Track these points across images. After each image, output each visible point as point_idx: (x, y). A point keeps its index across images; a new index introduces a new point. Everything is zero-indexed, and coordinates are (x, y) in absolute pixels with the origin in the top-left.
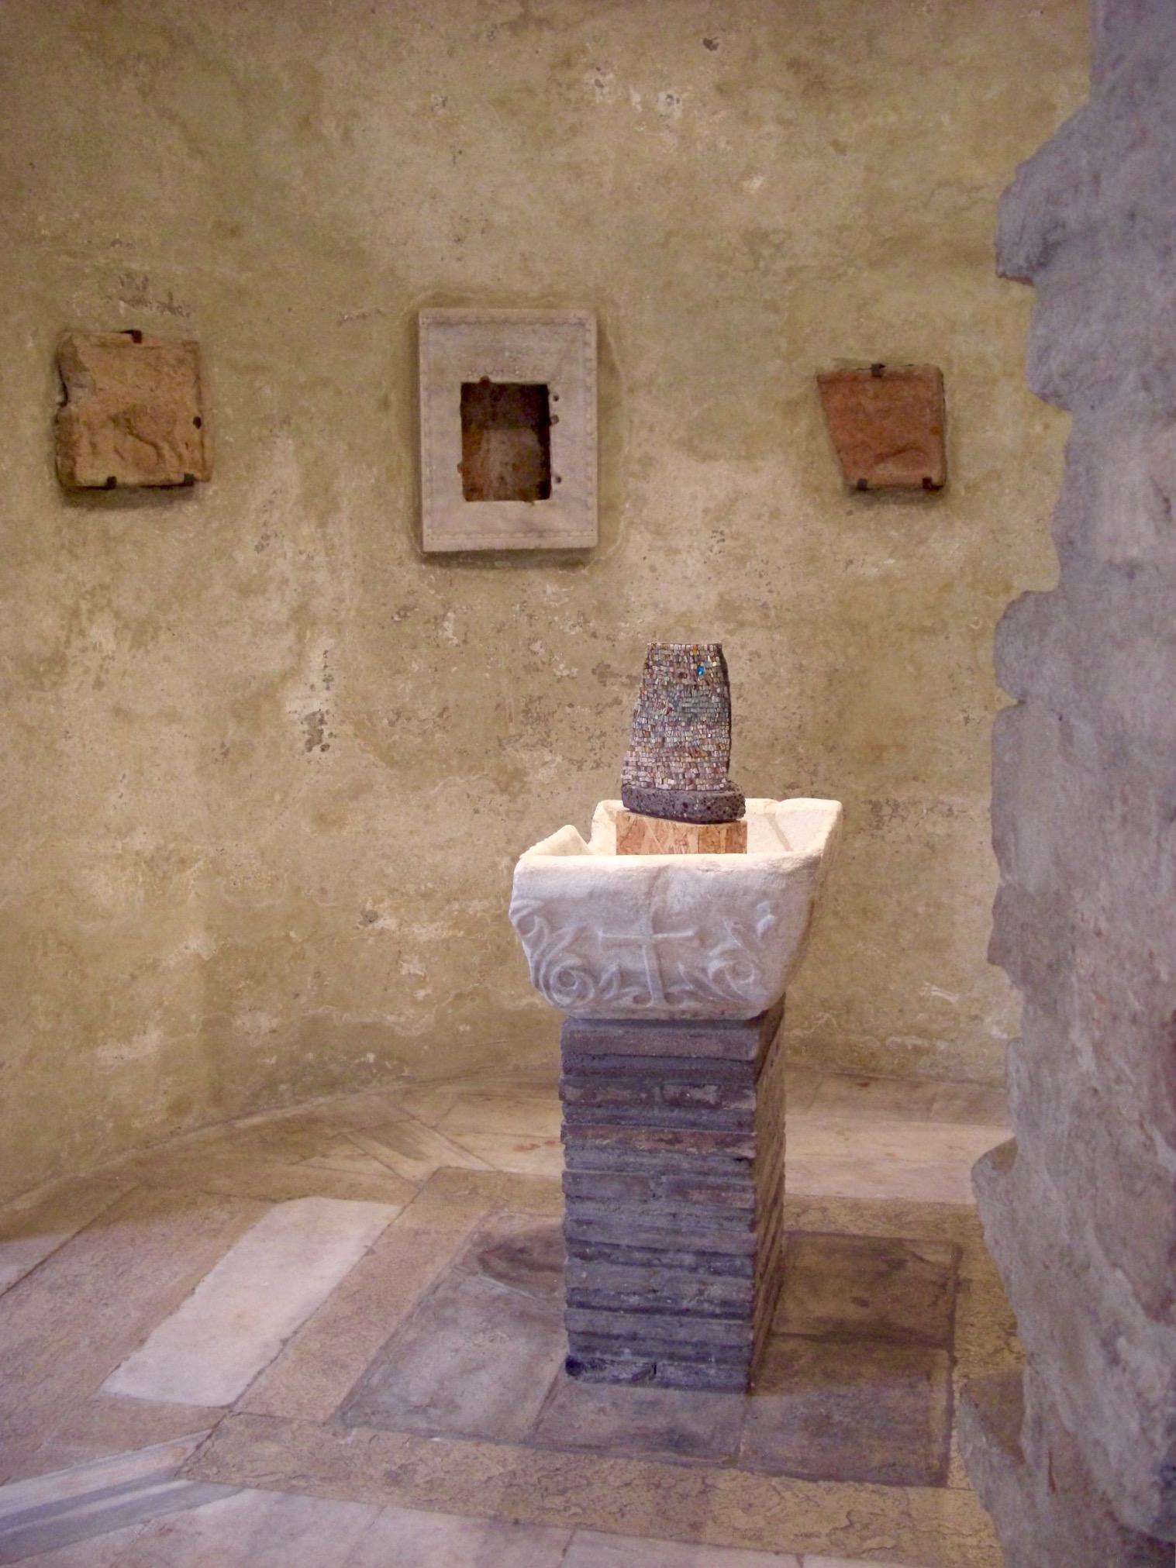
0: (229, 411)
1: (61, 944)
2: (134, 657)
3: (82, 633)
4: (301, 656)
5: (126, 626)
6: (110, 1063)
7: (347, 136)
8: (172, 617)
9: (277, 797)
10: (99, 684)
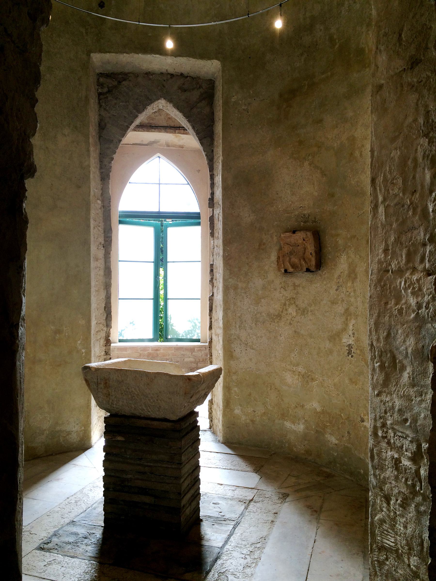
0: (330, 249)
1: (276, 389)
2: (301, 318)
3: (286, 310)
4: (347, 325)
5: (299, 309)
6: (288, 427)
7: (361, 155)
8: (312, 308)
9: (339, 369)
10: (290, 324)
